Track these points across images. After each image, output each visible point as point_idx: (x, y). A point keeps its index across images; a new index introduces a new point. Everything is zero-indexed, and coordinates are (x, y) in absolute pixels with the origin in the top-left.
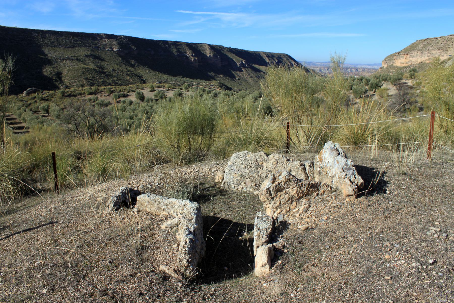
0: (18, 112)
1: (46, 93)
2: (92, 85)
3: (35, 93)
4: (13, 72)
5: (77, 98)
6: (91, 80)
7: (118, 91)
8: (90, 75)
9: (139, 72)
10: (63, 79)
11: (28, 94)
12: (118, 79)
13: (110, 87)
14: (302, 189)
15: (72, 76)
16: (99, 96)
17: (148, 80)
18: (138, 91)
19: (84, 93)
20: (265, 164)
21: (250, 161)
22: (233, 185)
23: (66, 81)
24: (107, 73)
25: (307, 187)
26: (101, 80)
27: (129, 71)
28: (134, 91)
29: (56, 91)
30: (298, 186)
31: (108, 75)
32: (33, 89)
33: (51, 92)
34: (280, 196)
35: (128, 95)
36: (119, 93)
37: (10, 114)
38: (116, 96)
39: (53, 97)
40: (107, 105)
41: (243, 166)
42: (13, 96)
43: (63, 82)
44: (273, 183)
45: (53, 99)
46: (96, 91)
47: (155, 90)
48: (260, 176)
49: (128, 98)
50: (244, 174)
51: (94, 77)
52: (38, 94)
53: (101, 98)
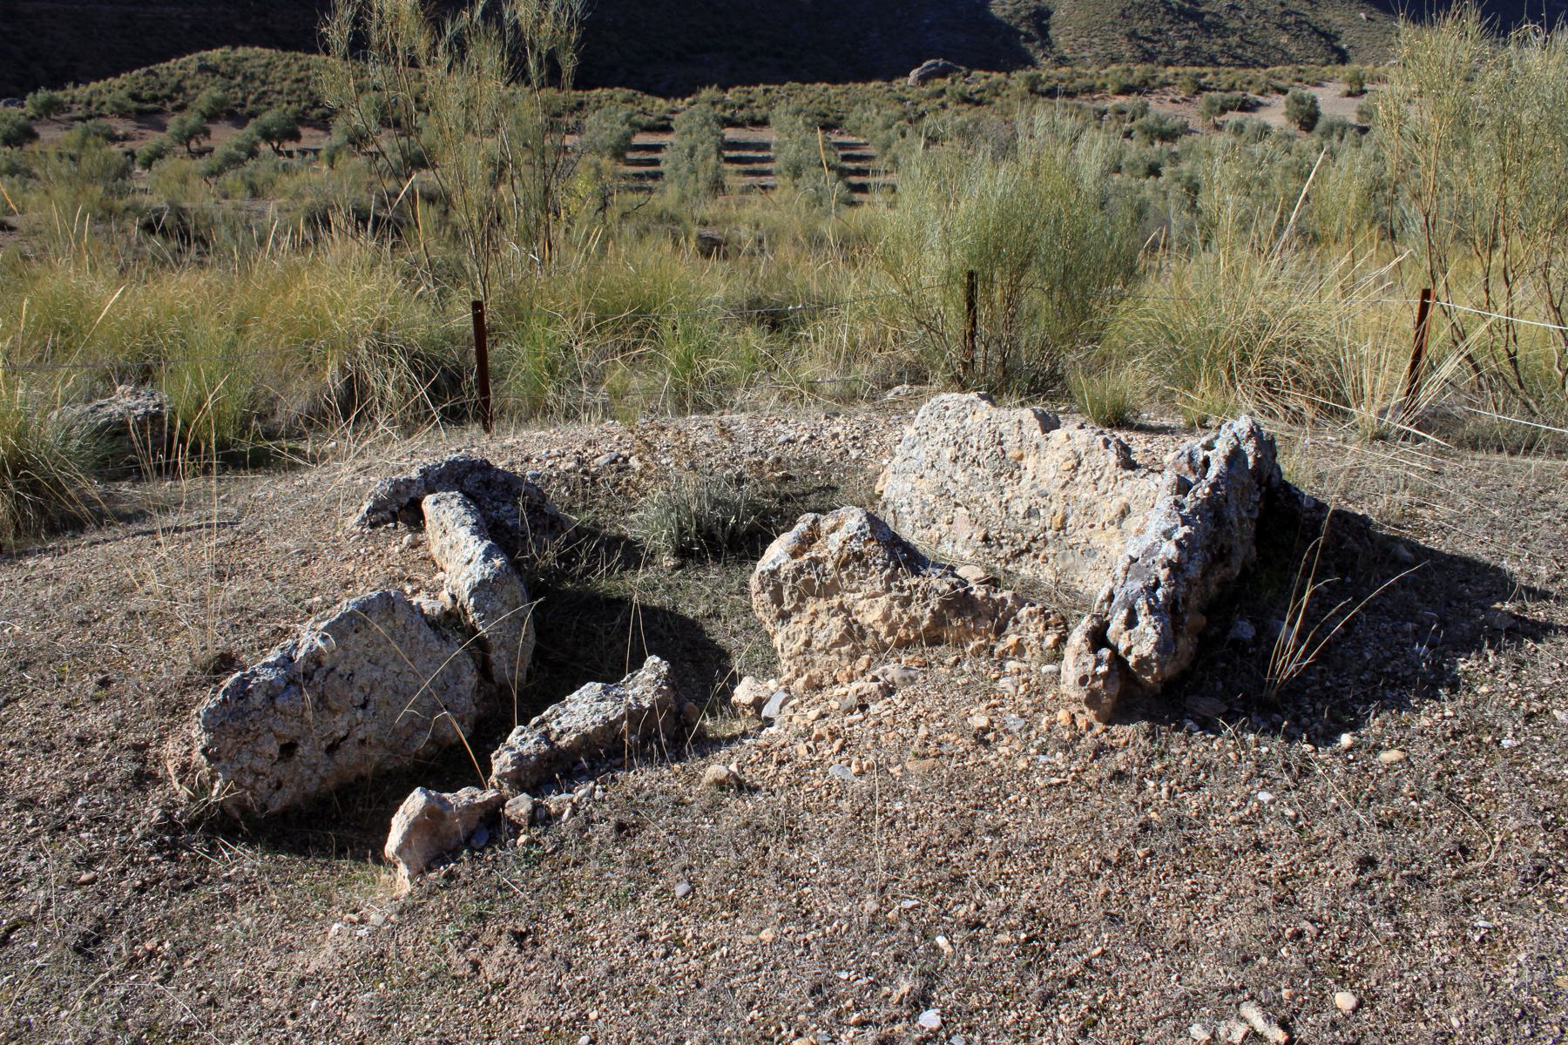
0: (881, 136)
1: (980, 79)
2: (1148, 57)
3: (944, 76)
4: (582, 24)
5: (1075, 101)
6: (1147, 40)
7: (1224, 86)
8: (1147, 23)
9: (1327, 17)
10: (1051, 32)
11: (923, 79)
12: (1245, 42)
13: (1197, 69)
14: (915, 610)
15: (1083, 24)
16: (1152, 101)
17: (1358, 50)
18: (1297, 90)
19: (1104, 86)
20: (1029, 462)
21: (974, 439)
22: (909, 520)
23: (1062, 40)
24: (1207, 18)
25: (934, 602)
26: (1181, 44)
27: (1289, 13)
28: (1283, 91)
29: (1013, 74)
30: (894, 593)
31: (1210, 24)
32: (941, 62)
33: (996, 76)
34: (815, 614)
35: (1259, 104)
36: (1227, 96)
37: (862, 141)
38: (1212, 103)
39: (997, 95)
40: (1169, 136)
41: (948, 453)
42: (879, 83)
43: (1050, 43)
44: (794, 555)
45: (998, 101)
46: (1145, 82)
47: (1363, 92)
48: (1005, 506)
49: (1255, 116)
50: (950, 485)
51: (1160, 32)
52: (953, 82)
53: (1161, 107)
